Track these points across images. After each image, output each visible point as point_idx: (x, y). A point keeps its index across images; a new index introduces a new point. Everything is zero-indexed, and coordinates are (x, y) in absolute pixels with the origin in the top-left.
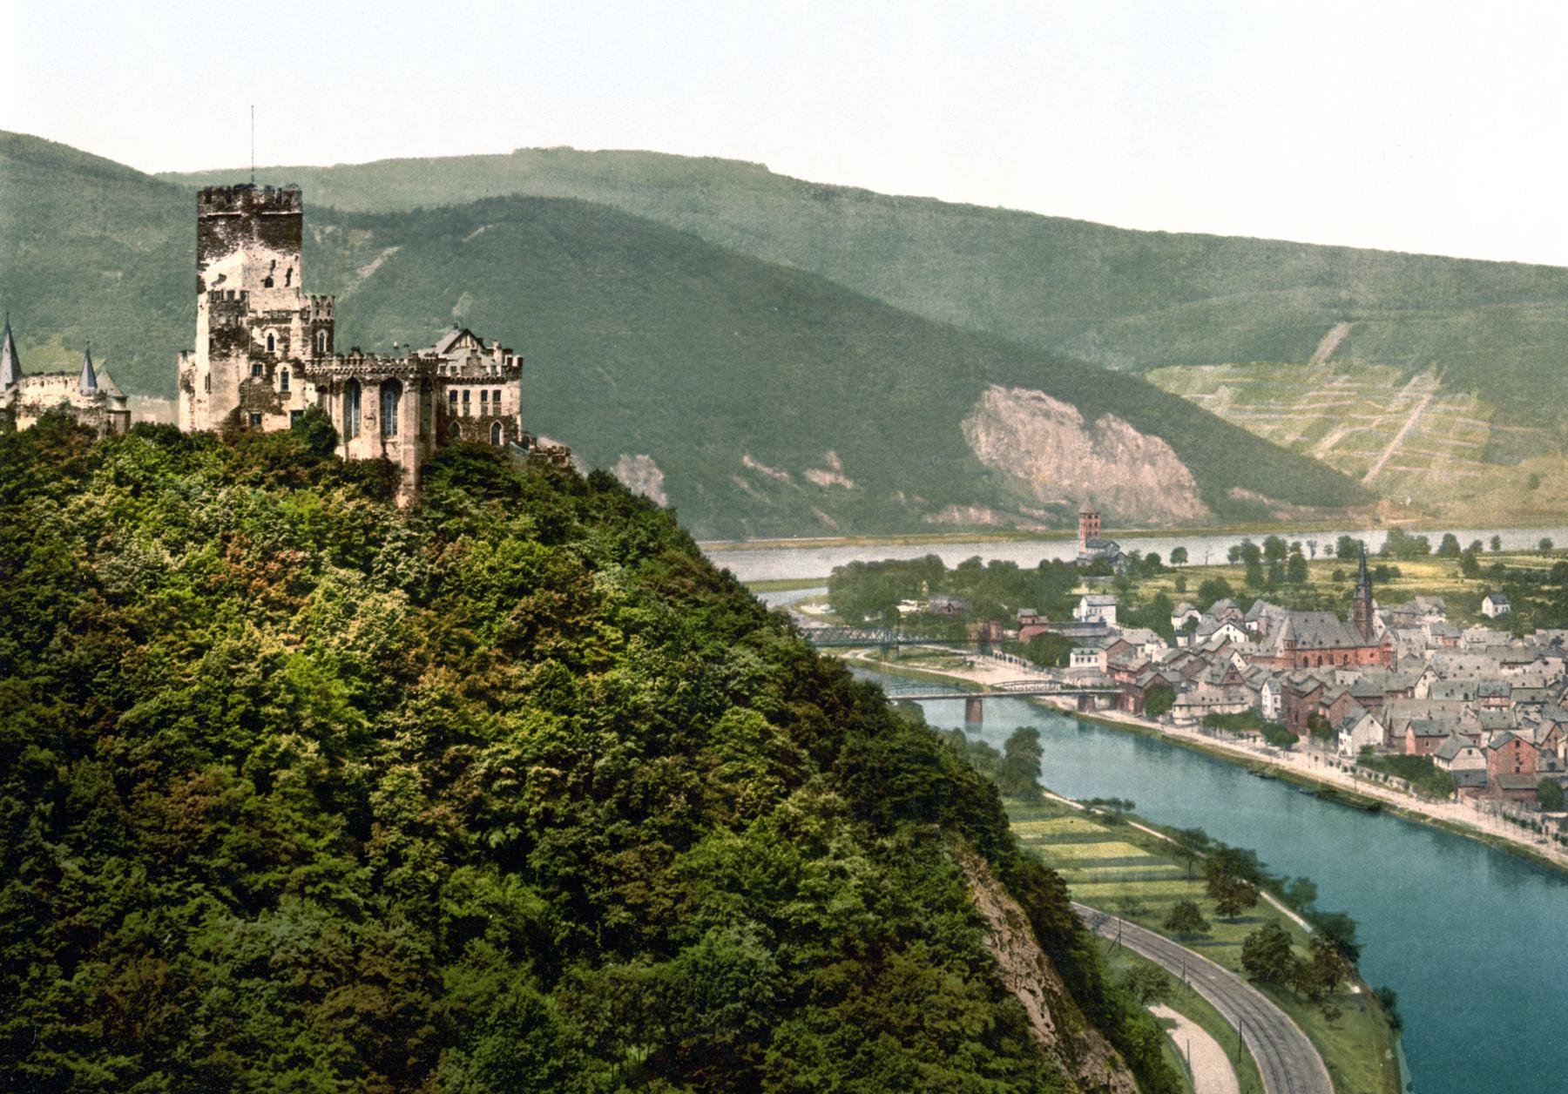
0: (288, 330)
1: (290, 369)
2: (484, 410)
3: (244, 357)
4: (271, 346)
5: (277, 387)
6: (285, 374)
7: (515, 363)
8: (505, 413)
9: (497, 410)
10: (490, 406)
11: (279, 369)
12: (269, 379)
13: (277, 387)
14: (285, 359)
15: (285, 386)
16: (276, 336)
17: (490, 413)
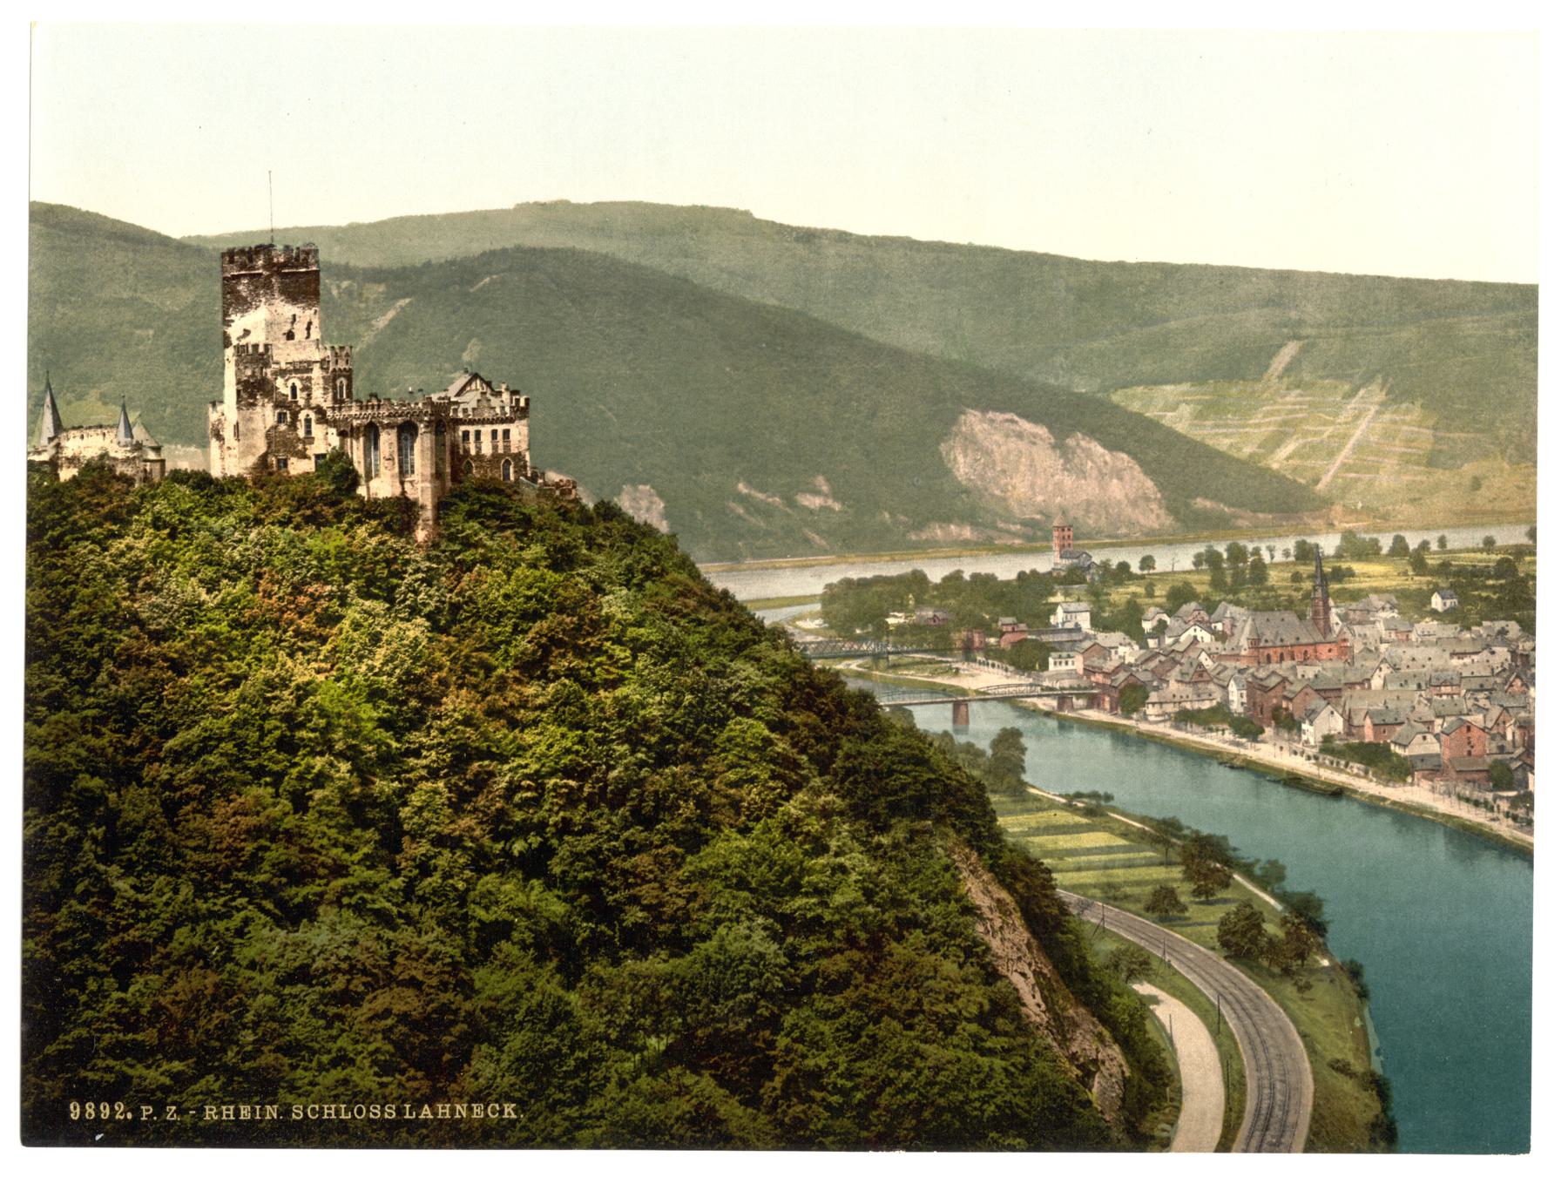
0: (309, 379)
1: (313, 416)
2: (495, 448)
3: (270, 406)
4: (294, 395)
5: (301, 433)
6: (308, 421)
7: (522, 404)
8: (514, 450)
9: (507, 447)
10: (501, 444)
11: (302, 416)
12: (293, 426)
13: (301, 433)
14: (308, 406)
15: (308, 432)
16: (299, 385)
17: (501, 451)
